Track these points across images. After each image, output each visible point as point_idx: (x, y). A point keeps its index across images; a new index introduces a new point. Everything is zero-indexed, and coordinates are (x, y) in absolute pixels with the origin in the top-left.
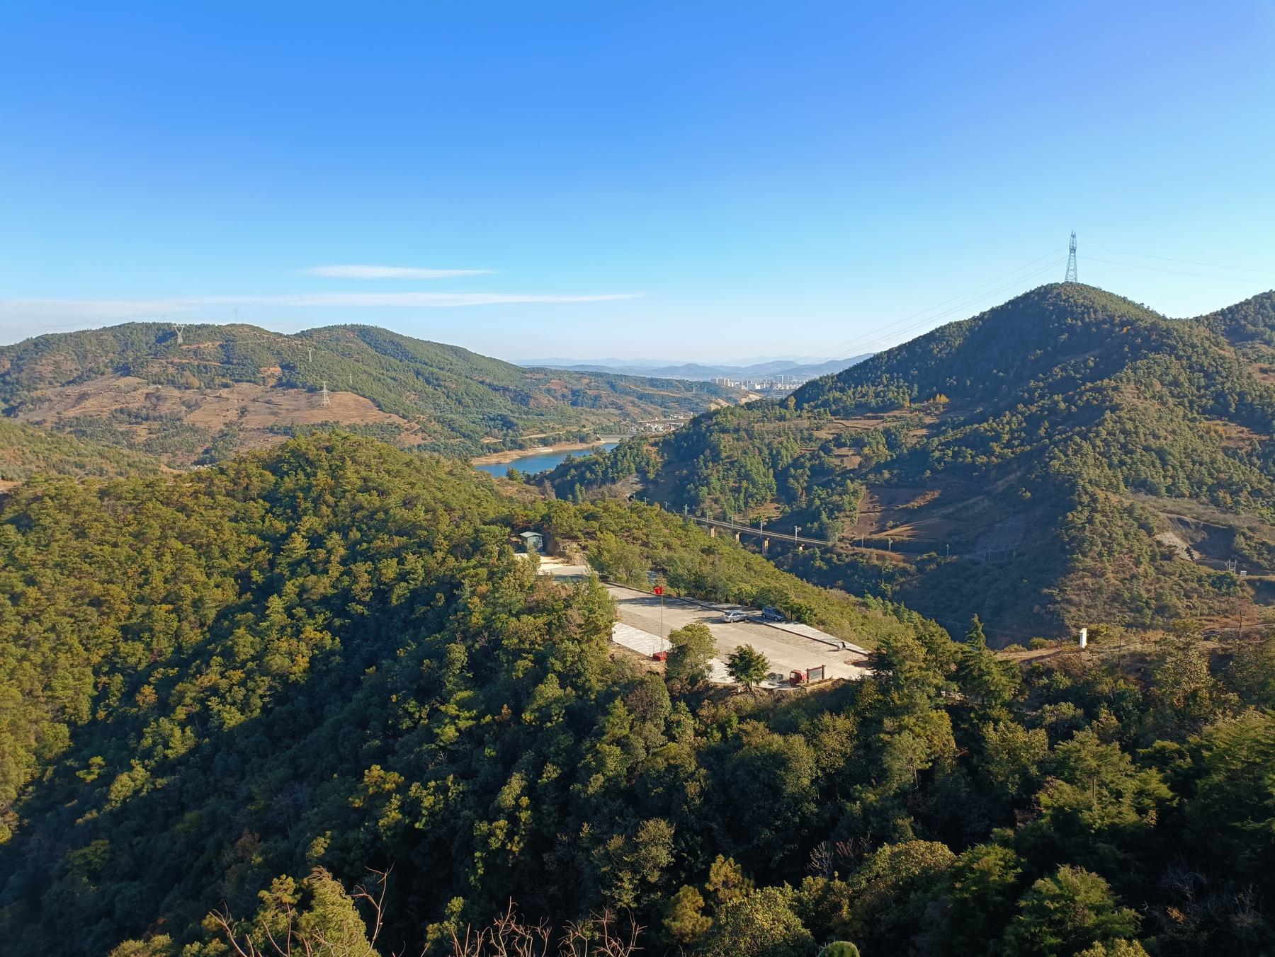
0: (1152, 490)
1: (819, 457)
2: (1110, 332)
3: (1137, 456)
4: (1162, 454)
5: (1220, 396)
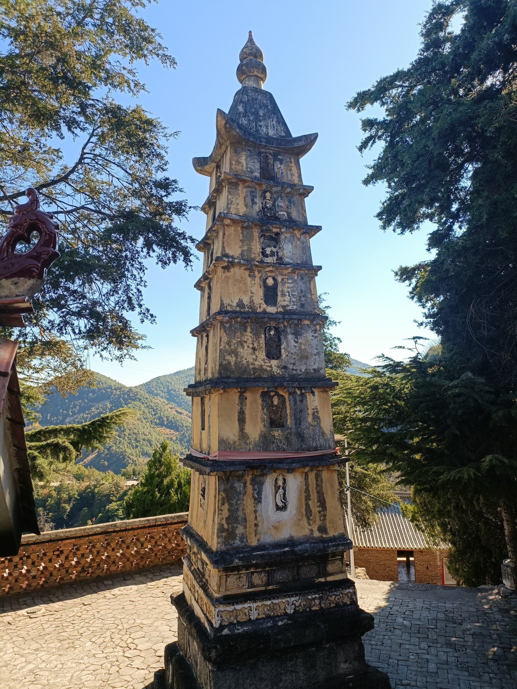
2: (112, 393)
3: (141, 443)
4: (149, 441)
5: (160, 418)
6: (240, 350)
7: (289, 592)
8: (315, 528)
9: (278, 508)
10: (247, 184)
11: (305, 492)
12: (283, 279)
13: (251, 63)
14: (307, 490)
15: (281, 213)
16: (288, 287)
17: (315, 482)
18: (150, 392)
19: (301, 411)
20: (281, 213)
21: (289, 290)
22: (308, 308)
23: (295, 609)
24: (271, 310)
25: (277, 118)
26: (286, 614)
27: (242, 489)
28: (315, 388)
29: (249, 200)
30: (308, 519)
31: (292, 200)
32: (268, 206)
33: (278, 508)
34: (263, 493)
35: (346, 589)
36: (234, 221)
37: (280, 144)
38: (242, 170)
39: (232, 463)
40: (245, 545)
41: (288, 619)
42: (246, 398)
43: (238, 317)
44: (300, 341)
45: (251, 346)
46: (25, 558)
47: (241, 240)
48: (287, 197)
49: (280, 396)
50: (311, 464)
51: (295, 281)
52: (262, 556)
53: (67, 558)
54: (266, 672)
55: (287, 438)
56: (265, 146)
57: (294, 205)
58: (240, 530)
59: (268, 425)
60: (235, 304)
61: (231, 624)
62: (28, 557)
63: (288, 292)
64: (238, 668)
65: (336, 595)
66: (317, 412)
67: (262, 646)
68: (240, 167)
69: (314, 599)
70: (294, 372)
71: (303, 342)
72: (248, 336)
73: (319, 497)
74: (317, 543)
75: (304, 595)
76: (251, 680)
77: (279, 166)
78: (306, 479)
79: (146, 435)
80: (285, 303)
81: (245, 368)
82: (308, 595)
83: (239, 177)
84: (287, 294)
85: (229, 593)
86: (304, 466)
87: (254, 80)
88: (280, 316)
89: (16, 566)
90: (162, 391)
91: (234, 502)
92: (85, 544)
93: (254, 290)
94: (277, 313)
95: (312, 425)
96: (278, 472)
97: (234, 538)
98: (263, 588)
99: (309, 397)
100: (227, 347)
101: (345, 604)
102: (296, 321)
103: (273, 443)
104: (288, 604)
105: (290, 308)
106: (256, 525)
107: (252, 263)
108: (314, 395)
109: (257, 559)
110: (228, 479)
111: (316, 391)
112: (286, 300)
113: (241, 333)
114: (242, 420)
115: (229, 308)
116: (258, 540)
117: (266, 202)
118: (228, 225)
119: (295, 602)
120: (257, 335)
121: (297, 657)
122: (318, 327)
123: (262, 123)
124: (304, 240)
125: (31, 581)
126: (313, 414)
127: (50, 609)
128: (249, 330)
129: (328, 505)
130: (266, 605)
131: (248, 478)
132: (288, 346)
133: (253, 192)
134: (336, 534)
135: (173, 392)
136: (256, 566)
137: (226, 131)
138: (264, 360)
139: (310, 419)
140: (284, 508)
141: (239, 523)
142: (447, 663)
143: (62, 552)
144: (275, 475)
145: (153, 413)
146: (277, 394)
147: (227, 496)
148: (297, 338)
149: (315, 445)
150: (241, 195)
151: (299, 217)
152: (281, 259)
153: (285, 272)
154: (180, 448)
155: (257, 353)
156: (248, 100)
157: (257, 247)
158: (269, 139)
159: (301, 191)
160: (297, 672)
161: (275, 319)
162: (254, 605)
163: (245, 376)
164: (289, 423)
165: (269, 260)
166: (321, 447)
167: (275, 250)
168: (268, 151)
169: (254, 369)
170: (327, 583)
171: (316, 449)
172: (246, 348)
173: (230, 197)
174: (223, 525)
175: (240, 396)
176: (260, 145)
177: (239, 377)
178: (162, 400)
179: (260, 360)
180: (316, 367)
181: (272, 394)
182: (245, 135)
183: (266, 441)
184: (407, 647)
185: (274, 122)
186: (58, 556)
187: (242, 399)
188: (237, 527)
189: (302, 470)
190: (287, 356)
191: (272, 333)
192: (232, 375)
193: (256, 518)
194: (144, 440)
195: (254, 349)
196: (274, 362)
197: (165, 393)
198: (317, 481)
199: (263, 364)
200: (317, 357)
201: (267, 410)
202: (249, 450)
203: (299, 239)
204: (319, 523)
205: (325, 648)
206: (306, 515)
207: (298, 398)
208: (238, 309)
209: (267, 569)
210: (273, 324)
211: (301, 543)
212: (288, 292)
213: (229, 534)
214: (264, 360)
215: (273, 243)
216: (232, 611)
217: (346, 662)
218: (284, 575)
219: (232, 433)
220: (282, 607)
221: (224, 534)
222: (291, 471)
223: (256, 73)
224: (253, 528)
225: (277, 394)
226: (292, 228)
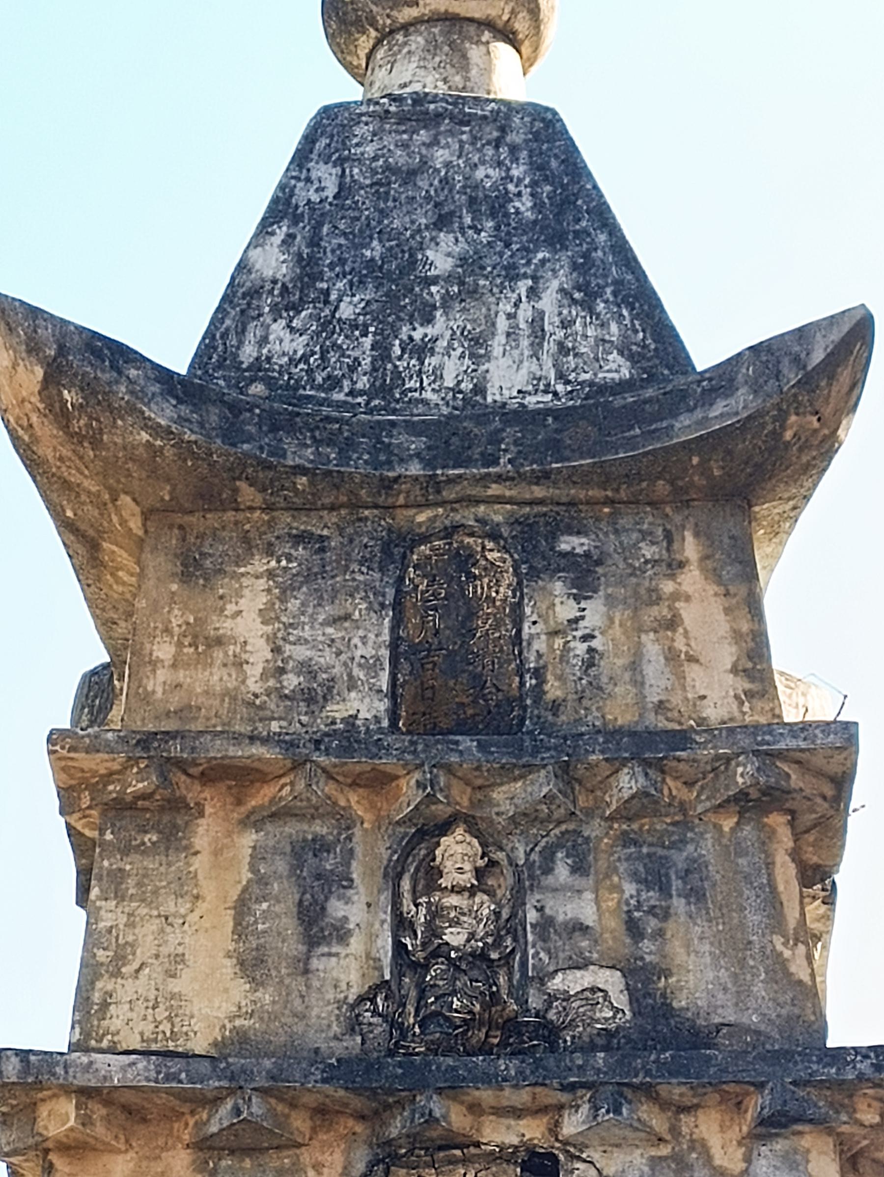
10: (261, 797)
15: (572, 982)
20: (572, 982)
25: (583, 266)
29: (278, 919)
32: (455, 937)
37: (555, 447)
38: (231, 695)
48: (626, 840)
56: (433, 484)
57: (696, 895)
68: (216, 677)
77: (566, 610)
83: (175, 749)
87: (432, 47)
117: (436, 912)
133: (320, 846)
137: (75, 438)
150: (208, 888)
151: (742, 994)
156: (343, 191)
158: (470, 431)
159: (743, 774)
168: (467, 516)
173: (111, 915)
176: (388, 485)
185: (548, 302)
226: (648, 1091)
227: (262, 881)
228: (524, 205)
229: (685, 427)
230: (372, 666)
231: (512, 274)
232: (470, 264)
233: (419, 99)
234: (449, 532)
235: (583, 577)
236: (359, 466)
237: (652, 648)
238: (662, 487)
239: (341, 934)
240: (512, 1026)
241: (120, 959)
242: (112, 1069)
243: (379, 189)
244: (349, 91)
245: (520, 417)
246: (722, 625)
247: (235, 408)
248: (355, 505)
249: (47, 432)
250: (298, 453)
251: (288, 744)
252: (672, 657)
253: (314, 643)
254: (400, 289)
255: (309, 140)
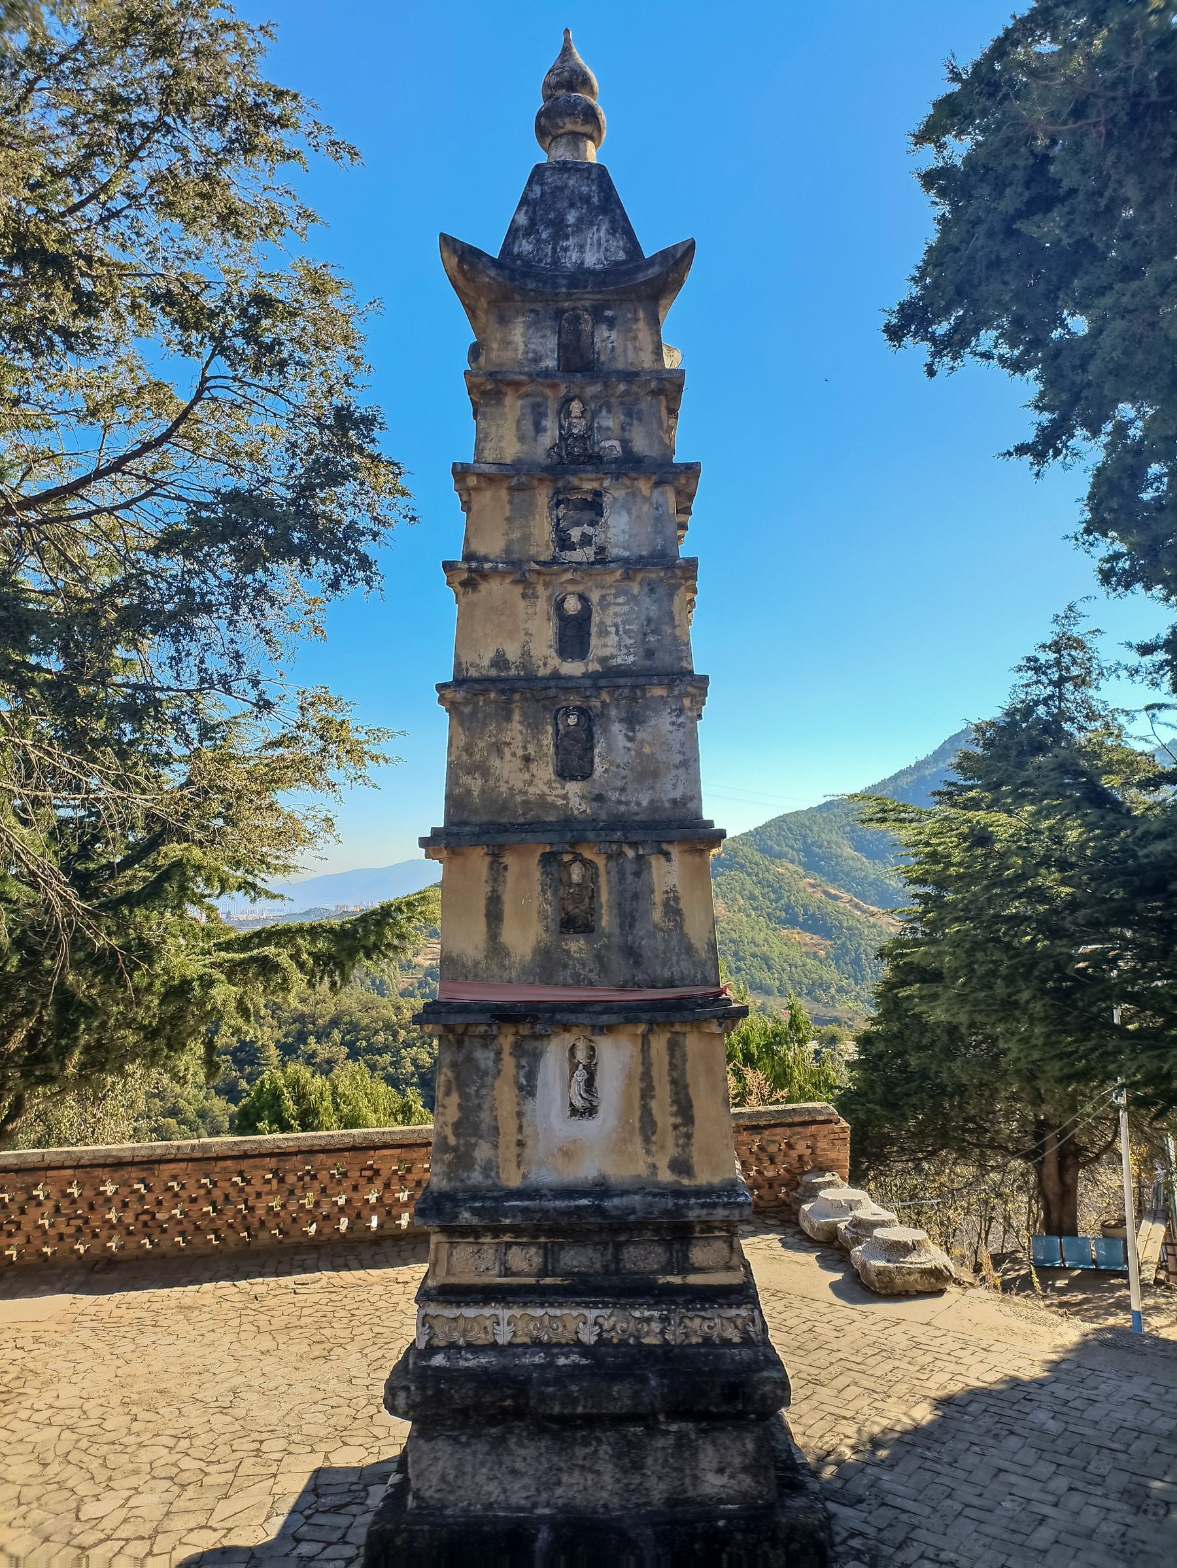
0: (768, 992)
1: (428, 984)
3: (748, 963)
4: (766, 959)
5: (788, 908)
6: (495, 762)
7: (589, 1296)
8: (663, 1163)
9: (574, 1111)
10: (523, 390)
11: (642, 1080)
12: (603, 597)
13: (566, 106)
14: (646, 1076)
15: (608, 444)
16: (616, 614)
17: (667, 1058)
18: (766, 851)
19: (636, 896)
20: (608, 444)
21: (619, 620)
22: (664, 660)
23: (599, 1335)
24: (572, 668)
25: (613, 221)
26: (579, 1343)
27: (491, 1064)
28: (670, 842)
29: (528, 425)
30: (647, 1140)
31: (636, 409)
32: (575, 431)
33: (574, 1111)
34: (540, 1076)
35: (730, 1306)
36: (490, 479)
39: (465, 1009)
40: (495, 1184)
41: (582, 1355)
42: (506, 868)
43: (487, 691)
44: (639, 735)
45: (520, 752)
46: (307, 1178)
47: (507, 519)
49: (587, 864)
50: (645, 1016)
51: (634, 599)
52: (525, 1211)
53: (387, 1186)
54: (525, 1459)
55: (599, 958)
57: (640, 419)
58: (483, 1152)
59: (554, 926)
60: (486, 662)
61: (452, 1345)
62: (314, 1177)
63: (616, 625)
64: (464, 1439)
65: (704, 1318)
66: (676, 899)
67: (508, 1402)
69: (648, 1320)
70: (622, 808)
71: (649, 739)
72: (515, 730)
73: (677, 1093)
74: (662, 1195)
75: (623, 1307)
76: (491, 1470)
77: (606, 334)
78: (645, 1049)
79: (757, 946)
80: (607, 652)
81: (506, 801)
82: (632, 1307)
83: (499, 377)
84: (613, 629)
85: (453, 1280)
86: (636, 1021)
87: (569, 143)
88: (588, 683)
89: (292, 1192)
90: (792, 848)
91: (472, 1090)
92: (422, 1161)
93: (532, 627)
94: (585, 675)
95: (661, 930)
96: (575, 1030)
97: (470, 1167)
98: (532, 1281)
99: (657, 865)
100: (465, 757)
101: (727, 1343)
102: (626, 692)
103: (565, 966)
104: (584, 1323)
105: (619, 661)
106: (520, 1144)
107: (526, 567)
108: (669, 860)
109: (514, 1217)
110: (460, 1043)
111: (674, 851)
112: (609, 645)
113: (499, 726)
114: (494, 916)
115: (473, 673)
116: (524, 1176)
117: (570, 424)
118: (477, 489)
119: (600, 1320)
120: (534, 727)
121: (599, 1441)
122: (687, 702)
123: (571, 242)
124: (661, 501)
125: (322, 1223)
126: (666, 904)
127: (335, 1281)
128: (517, 716)
129: (697, 1112)
130: (533, 1318)
131: (507, 1041)
132: (610, 749)
133: (539, 405)
134: (716, 1180)
135: (815, 849)
136: (515, 1230)
137: (468, 280)
138: (549, 783)
139: (657, 915)
140: (590, 1111)
141: (481, 1137)
142: (1090, 1535)
143: (377, 1172)
144: (569, 1039)
145: (773, 896)
146: (578, 858)
147: (457, 1078)
148: (633, 730)
149: (667, 974)
152: (601, 550)
153: (609, 579)
154: (837, 977)
155: (533, 767)
157: (542, 531)
158: (580, 277)
159: (653, 385)
160: (597, 1472)
161: (577, 689)
162: (504, 1313)
163: (504, 820)
164: (604, 923)
165: (578, 555)
166: (682, 979)
167: (590, 531)
168: (579, 304)
169: (526, 803)
170: (685, 1289)
171: (670, 984)
172: (508, 756)
173: (483, 425)
174: (446, 1137)
175: (492, 864)
176: (557, 294)
177: (491, 823)
178: (790, 866)
179: (540, 784)
180: (677, 794)
181: (567, 858)
182: (512, 279)
183: (548, 963)
184: (1013, 1479)
185: (602, 233)
186: (370, 1180)
187: (497, 870)
188: (476, 1144)
189: (630, 1029)
190: (606, 771)
191: (572, 720)
192: (474, 819)
193: (520, 1128)
194: (754, 955)
195: (527, 759)
196: (574, 788)
197: (798, 851)
198: (672, 1056)
199: (547, 791)
200: (681, 771)
201: (555, 893)
202: (510, 981)
203: (647, 500)
204: (672, 1151)
205: (668, 1432)
206: (643, 1129)
207: (630, 868)
208: (493, 673)
209: (543, 1240)
210: (575, 700)
211: (624, 1193)
212: (616, 625)
213: (458, 1157)
214: (549, 783)
215: (588, 515)
216: (455, 1319)
217: (721, 1471)
218: (583, 1259)
219: (471, 943)
220: (571, 1327)
221: (448, 1157)
222: (609, 1029)
223: (569, 127)
224: (514, 1149)
225: (578, 858)
226: (626, 475)
227: (523, 414)
228: (595, 200)
229: (641, 277)
230: (552, 351)
231: (592, 224)
232: (580, 220)
233: (565, 162)
234: (574, 309)
235: (611, 323)
236: (548, 290)
237: (630, 346)
238: (633, 296)
239: (545, 430)
240: (590, 457)
241: (486, 437)
242: (485, 468)
243: (553, 194)
244: (543, 158)
245: (592, 272)
246: (649, 339)
247: (513, 270)
248: (547, 301)
249: (459, 277)
250: (531, 285)
251: (530, 375)
252: (635, 348)
253: (537, 344)
254: (559, 230)
255: (532, 176)
